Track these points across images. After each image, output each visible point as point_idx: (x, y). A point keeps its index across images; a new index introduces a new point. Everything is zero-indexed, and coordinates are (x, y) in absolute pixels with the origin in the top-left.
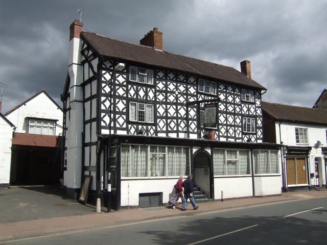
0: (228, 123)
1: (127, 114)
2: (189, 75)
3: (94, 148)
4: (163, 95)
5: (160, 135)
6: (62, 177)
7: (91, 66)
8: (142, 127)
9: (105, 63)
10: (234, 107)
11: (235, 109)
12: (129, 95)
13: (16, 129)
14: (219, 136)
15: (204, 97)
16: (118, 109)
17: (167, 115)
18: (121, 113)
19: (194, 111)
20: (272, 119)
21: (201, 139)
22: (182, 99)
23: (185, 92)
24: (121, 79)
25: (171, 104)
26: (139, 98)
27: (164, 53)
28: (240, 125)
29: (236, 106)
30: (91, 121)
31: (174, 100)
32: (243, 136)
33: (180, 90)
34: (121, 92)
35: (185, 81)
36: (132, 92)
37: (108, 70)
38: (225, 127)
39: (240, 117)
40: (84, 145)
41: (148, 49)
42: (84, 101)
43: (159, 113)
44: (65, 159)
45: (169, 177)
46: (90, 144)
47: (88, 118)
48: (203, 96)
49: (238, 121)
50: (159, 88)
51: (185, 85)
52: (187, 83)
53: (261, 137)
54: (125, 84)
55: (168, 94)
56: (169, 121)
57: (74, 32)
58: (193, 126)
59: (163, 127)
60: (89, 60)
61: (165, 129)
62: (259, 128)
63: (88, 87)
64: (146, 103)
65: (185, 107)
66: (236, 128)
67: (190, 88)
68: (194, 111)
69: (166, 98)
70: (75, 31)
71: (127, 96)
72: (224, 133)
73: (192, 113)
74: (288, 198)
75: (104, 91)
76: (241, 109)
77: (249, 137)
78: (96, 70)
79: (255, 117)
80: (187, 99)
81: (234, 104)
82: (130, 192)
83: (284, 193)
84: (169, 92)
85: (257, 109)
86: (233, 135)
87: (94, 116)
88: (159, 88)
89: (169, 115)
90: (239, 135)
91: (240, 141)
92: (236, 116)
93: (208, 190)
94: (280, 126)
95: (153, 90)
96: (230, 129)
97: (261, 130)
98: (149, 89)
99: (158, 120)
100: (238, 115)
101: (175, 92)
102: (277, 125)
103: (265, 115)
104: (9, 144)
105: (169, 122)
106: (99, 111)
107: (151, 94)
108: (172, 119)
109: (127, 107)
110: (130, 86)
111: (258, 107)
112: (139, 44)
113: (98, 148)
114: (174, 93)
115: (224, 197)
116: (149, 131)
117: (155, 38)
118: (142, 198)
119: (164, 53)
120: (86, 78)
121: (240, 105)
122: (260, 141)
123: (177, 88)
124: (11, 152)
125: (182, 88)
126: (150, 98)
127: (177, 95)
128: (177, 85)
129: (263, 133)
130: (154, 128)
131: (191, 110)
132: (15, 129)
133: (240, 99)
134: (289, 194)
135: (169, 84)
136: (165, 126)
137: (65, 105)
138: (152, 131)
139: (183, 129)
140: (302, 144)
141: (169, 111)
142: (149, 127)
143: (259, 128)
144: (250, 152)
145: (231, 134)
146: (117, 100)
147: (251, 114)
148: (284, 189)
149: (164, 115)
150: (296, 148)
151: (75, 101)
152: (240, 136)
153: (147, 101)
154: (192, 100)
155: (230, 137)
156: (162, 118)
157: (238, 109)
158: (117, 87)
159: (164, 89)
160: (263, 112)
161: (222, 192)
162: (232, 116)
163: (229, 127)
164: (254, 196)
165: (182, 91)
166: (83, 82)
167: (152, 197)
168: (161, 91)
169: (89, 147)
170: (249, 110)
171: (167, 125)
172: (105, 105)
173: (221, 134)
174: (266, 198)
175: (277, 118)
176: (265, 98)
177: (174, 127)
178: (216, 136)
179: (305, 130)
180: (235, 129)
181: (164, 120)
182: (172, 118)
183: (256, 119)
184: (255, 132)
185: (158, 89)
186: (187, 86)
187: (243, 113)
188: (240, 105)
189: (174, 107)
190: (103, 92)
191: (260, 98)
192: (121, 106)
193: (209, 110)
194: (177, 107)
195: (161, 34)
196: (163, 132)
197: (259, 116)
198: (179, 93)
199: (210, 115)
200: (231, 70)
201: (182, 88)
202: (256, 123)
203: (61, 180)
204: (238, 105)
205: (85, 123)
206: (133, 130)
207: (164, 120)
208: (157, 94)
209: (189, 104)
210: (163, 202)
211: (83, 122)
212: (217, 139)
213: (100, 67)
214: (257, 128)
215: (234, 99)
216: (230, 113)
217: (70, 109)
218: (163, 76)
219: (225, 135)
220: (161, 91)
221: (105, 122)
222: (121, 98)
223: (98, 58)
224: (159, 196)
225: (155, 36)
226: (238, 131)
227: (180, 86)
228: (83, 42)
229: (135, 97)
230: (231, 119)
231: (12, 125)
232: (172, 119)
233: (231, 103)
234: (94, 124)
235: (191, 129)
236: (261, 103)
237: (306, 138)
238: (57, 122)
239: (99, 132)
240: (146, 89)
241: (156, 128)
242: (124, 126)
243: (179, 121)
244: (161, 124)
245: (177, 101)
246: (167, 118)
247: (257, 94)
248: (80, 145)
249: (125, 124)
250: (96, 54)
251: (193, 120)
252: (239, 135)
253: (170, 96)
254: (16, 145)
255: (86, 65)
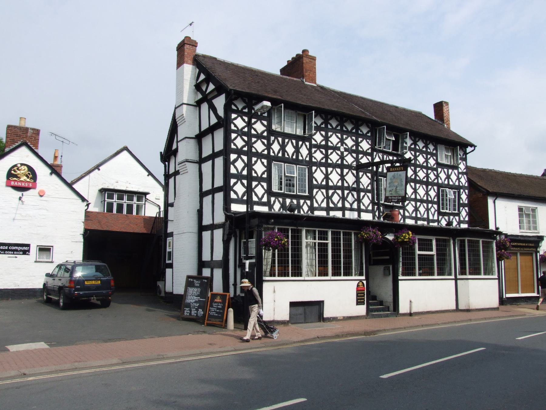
0: (418, 197)
1: (269, 180)
2: (360, 123)
3: (219, 234)
4: (321, 152)
5: (317, 213)
6: (162, 276)
7: (212, 108)
8: (292, 202)
9: (235, 102)
10: (427, 172)
11: (427, 176)
12: (271, 151)
13: (90, 205)
14: (404, 217)
15: (383, 157)
16: (256, 172)
17: (327, 183)
18: (260, 179)
19: (368, 177)
20: (483, 192)
21: (374, 220)
22: (349, 159)
23: (354, 148)
24: (259, 127)
25: (334, 166)
26: (286, 156)
27: (319, 88)
28: (436, 200)
29: (430, 171)
30: (213, 191)
31: (338, 161)
32: (440, 217)
33: (346, 145)
34: (259, 146)
35: (354, 131)
36: (276, 147)
37: (240, 113)
38: (413, 203)
39: (435, 188)
40: (202, 228)
41: (295, 81)
42: (201, 161)
43: (316, 180)
44: (168, 250)
45: (307, 278)
46: (212, 227)
47: (207, 186)
48: (380, 155)
49: (432, 193)
50: (316, 141)
51: (354, 138)
52: (357, 135)
53: (467, 219)
54: (265, 134)
55: (330, 151)
56: (331, 192)
57: (184, 55)
58: (366, 201)
59: (323, 201)
60: (209, 97)
61: (324, 205)
62: (464, 205)
63: (207, 143)
64: (296, 165)
65: (355, 172)
66: (430, 205)
67: (361, 141)
68: (368, 177)
69: (327, 156)
70: (186, 53)
71: (269, 152)
72: (412, 213)
73: (365, 181)
74: (508, 314)
75: (235, 145)
76: (437, 176)
77: (449, 219)
78: (221, 113)
79: (457, 188)
80: (357, 159)
81: (427, 168)
82: (278, 297)
83: (502, 306)
84: (331, 148)
85: (460, 176)
86: (425, 216)
87: (219, 182)
88: (316, 141)
89: (331, 184)
90: (433, 215)
91: (435, 224)
92: (430, 187)
93: (388, 298)
94: (494, 202)
95: (307, 144)
96: (420, 206)
97: (467, 208)
98: (300, 143)
99: (315, 191)
100: (433, 184)
101: (339, 147)
102: (490, 201)
103: (472, 186)
104: (80, 229)
105: (330, 195)
106: (227, 175)
107: (304, 151)
108: (335, 190)
109: (269, 170)
110: (272, 138)
111: (463, 173)
112: (278, 73)
113: (227, 232)
114: (339, 149)
115: (414, 310)
116: (302, 207)
117: (304, 65)
118: (293, 308)
119: (319, 88)
120: (205, 126)
121: (436, 170)
122: (464, 226)
123: (342, 141)
124: (82, 240)
125: (349, 142)
126: (302, 156)
127: (342, 153)
128: (342, 136)
129: (469, 214)
130: (309, 202)
131: (363, 175)
132: (88, 205)
133: (436, 160)
134: (508, 307)
135: (331, 136)
136: (325, 200)
137: (167, 169)
138: (306, 208)
139: (351, 205)
140: (530, 233)
141: (330, 176)
142: (302, 201)
143: (464, 205)
144: (452, 242)
145: (422, 213)
146: (254, 159)
147: (451, 183)
148: (503, 301)
149: (324, 183)
150: (519, 238)
151: (187, 161)
152: (436, 218)
153: (296, 162)
154: (364, 160)
155: (420, 219)
156: (320, 187)
157: (432, 176)
158: (254, 140)
159: (323, 143)
160: (469, 181)
161: (411, 301)
162: (424, 186)
163: (418, 204)
164: (457, 310)
165: (350, 147)
166: (208, 126)
167: (308, 309)
168: (318, 147)
169: (209, 232)
170: (448, 177)
171: (328, 198)
172: (235, 167)
173: (407, 214)
174: (477, 313)
175: (490, 191)
176: (476, 160)
177: (338, 202)
178: (400, 217)
179: (534, 210)
180: (428, 206)
181: (324, 191)
182: (335, 188)
183: (459, 192)
184: (457, 212)
185: (314, 142)
186: (357, 139)
187: (440, 182)
188: (436, 170)
189: (339, 170)
190: (233, 146)
191: (465, 159)
192: (259, 168)
193: (394, 176)
194: (342, 172)
195: (314, 59)
196: (322, 209)
197: (463, 187)
198: (346, 150)
199: (396, 184)
200: (419, 116)
201: (349, 142)
202: (459, 198)
203: (160, 284)
204: (433, 169)
205: (203, 194)
206: (277, 207)
207: (324, 191)
208: (313, 150)
209: (360, 167)
210: (325, 316)
211: (198, 193)
212: (402, 221)
213: (227, 108)
214: (460, 205)
215: (427, 161)
216: (421, 182)
217: (177, 173)
218: (322, 124)
219: (414, 215)
220: (318, 147)
221: (236, 193)
222: (259, 156)
223: (4, 140)
224: (318, 306)
225: (304, 61)
226: (433, 210)
227: (346, 138)
228: (198, 70)
229: (280, 155)
230: (421, 191)
231: (83, 199)
232: (335, 190)
233: (422, 167)
234: (219, 197)
235: (364, 205)
236: (467, 167)
237: (535, 222)
238: (148, 196)
239: (227, 208)
240: (297, 143)
241: (312, 203)
242: (265, 199)
243: (346, 192)
244: (319, 196)
245: (342, 162)
246: (327, 187)
247: (460, 153)
248: (195, 229)
249: (266, 196)
250: (220, 89)
251: (366, 191)
252: (433, 215)
253: (332, 153)
254: (91, 231)
255: (205, 107)
